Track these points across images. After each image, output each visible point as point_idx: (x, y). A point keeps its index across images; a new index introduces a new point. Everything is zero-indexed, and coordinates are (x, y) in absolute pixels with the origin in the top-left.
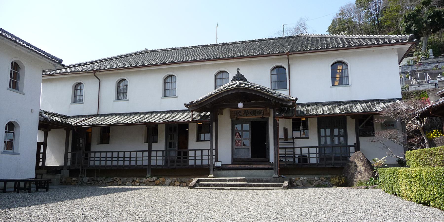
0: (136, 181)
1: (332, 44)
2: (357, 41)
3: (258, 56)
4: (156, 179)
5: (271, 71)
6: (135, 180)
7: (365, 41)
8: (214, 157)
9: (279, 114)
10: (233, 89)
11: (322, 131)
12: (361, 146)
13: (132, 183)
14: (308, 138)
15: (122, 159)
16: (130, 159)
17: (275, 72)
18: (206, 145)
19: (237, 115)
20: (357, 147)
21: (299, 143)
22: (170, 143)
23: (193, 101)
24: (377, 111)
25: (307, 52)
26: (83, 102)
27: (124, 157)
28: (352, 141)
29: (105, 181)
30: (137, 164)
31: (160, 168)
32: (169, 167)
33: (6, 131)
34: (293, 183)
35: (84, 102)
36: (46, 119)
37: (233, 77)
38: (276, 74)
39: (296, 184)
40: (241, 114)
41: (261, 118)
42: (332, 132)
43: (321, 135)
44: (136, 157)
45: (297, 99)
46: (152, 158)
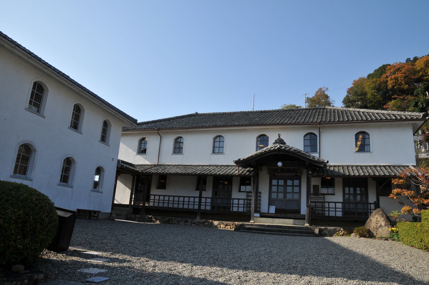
0: (189, 221)
1: (356, 117)
2: (377, 116)
4: (205, 221)
5: (304, 137)
6: (188, 220)
7: (384, 116)
9: (312, 173)
11: (347, 189)
12: (381, 205)
14: (334, 194)
15: (172, 202)
16: (169, 202)
17: (308, 137)
20: (377, 205)
21: (328, 198)
23: (240, 159)
24: (395, 175)
25: (336, 123)
27: (179, 201)
28: (372, 199)
31: (209, 212)
33: (62, 174)
34: (322, 232)
35: (184, 154)
36: (122, 166)
37: (275, 141)
38: (309, 140)
39: (324, 233)
40: (278, 171)
41: (295, 175)
42: (355, 191)
43: (346, 193)
44: (179, 201)
45: (328, 162)
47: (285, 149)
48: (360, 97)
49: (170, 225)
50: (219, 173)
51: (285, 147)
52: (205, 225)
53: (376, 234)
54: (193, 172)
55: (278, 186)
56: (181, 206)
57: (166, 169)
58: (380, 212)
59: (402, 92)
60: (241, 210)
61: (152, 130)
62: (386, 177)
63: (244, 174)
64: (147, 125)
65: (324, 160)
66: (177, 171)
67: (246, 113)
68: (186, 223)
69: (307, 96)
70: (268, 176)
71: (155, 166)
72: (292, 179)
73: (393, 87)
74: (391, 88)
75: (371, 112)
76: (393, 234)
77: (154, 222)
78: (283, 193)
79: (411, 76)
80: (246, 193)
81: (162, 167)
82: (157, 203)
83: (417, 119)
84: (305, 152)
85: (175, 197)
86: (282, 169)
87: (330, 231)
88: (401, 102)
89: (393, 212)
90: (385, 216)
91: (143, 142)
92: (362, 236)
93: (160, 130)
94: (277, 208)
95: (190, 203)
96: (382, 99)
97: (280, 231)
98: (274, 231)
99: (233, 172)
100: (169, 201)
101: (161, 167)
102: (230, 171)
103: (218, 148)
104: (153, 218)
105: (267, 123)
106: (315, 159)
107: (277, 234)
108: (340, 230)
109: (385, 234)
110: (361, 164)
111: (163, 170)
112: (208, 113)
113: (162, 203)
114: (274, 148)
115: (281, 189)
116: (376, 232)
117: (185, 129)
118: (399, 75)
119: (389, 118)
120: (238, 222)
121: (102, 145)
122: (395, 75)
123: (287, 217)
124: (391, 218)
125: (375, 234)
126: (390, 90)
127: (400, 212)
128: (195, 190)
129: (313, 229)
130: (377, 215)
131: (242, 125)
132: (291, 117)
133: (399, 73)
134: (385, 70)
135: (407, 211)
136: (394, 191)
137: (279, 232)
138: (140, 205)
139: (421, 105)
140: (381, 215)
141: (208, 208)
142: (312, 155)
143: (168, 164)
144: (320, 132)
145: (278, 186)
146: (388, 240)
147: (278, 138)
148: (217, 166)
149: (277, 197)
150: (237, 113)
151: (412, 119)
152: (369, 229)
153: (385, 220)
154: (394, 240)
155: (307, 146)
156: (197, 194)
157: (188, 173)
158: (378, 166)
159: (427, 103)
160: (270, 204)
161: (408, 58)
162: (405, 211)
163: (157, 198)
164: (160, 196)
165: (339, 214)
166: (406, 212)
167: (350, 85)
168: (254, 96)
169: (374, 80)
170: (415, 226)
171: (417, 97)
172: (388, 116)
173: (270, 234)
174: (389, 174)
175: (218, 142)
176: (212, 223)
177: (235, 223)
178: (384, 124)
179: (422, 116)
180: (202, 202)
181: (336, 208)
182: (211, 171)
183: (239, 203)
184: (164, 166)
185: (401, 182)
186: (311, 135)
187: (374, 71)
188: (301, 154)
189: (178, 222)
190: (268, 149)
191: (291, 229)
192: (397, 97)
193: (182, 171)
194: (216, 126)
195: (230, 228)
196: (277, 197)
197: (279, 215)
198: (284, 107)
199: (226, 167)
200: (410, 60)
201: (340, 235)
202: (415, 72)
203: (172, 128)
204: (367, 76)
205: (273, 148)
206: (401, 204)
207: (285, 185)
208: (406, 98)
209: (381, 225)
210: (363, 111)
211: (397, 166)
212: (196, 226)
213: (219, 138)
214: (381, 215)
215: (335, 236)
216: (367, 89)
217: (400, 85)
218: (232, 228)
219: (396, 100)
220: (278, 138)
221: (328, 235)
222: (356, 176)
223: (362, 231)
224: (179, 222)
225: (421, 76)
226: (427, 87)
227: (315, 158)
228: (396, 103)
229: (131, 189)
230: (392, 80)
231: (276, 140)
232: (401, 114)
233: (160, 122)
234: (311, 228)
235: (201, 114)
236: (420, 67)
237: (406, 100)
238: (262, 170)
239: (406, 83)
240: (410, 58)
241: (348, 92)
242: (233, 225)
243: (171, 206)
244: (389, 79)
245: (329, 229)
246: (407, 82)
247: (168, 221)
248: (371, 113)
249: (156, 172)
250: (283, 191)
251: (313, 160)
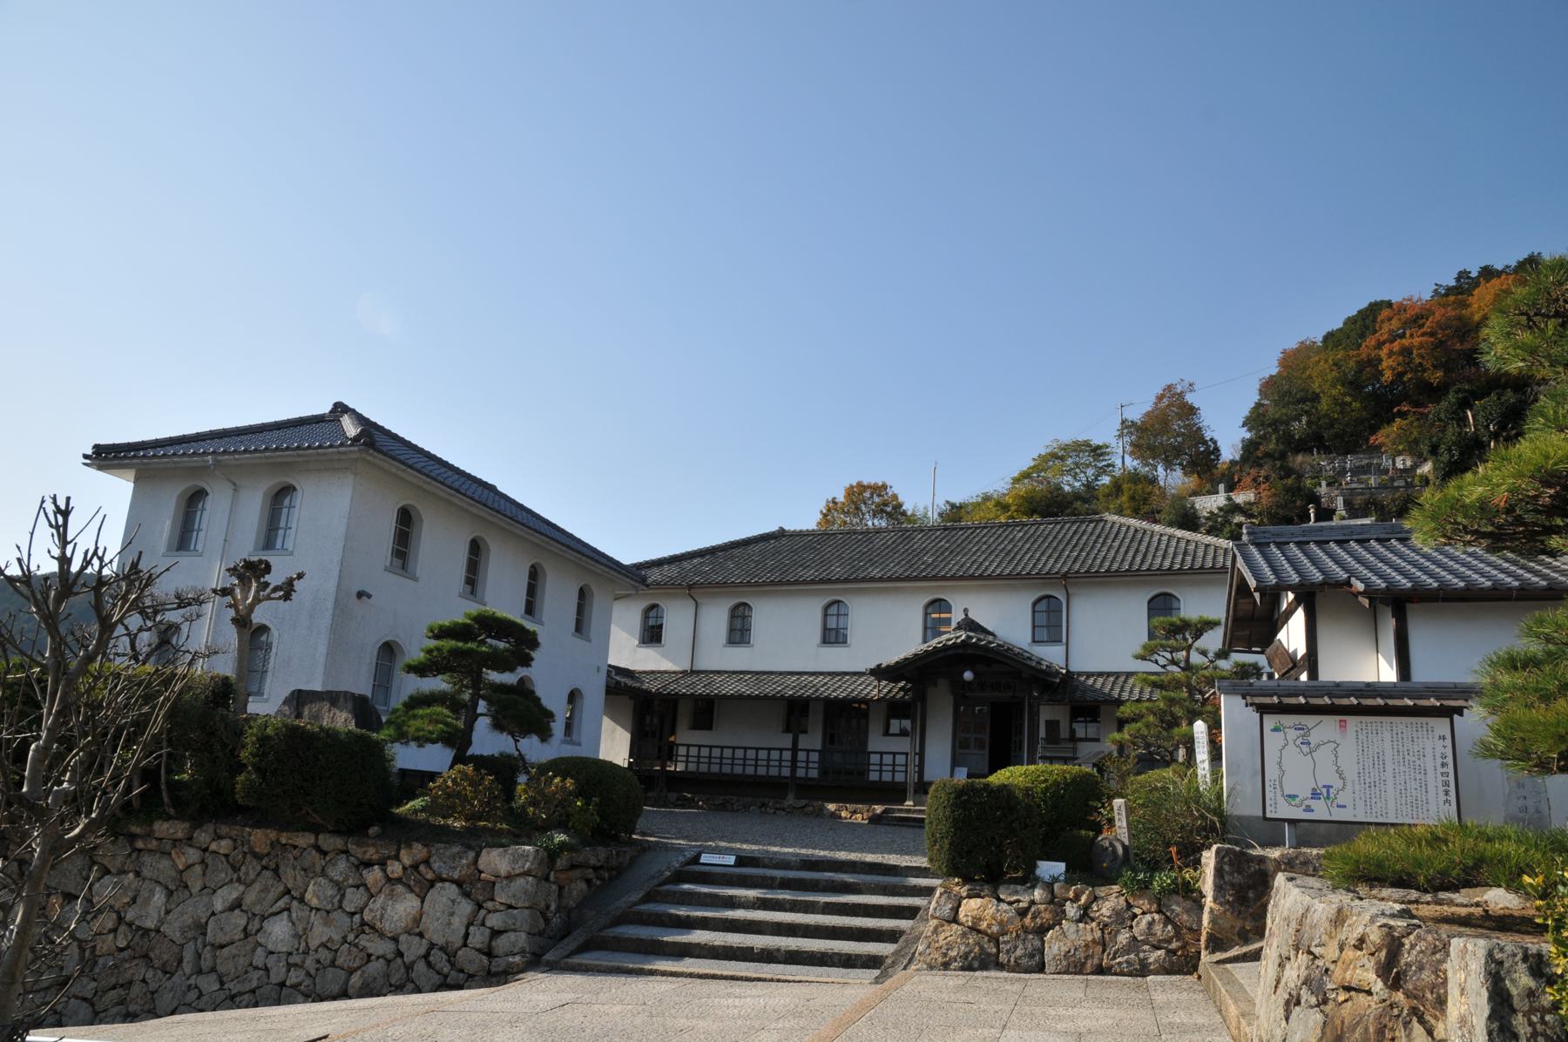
3: (1009, 577)
8: (917, 769)
17: (1042, 606)
18: (903, 745)
22: (832, 736)
27: (721, 758)
36: (618, 683)
44: (757, 760)
56: (750, 770)
68: (763, 809)
70: (951, 699)
82: (695, 765)
91: (651, 614)
118: (1417, 340)
121: (580, 642)
141: (814, 774)
156: (786, 741)
161: (1462, 269)
163: (693, 751)
164: (700, 747)
176: (822, 809)
181: (733, 759)
182: (818, 689)
187: (1345, 323)
200: (1469, 278)
213: (835, 606)
224: (746, 807)
227: (1043, 662)
229: (630, 729)
242: (868, 811)
243: (726, 769)
251: (1038, 667)
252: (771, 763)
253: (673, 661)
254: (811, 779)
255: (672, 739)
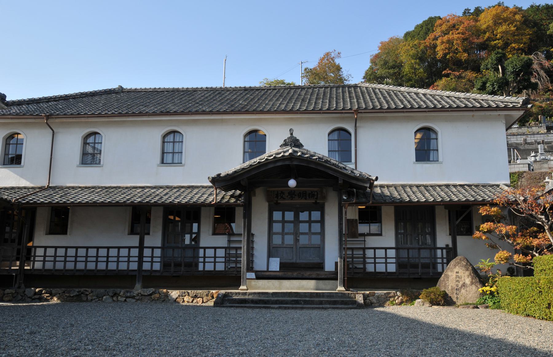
0: (120, 294)
4: (153, 292)
5: (329, 134)
6: (118, 292)
7: (461, 101)
9: (347, 198)
10: (283, 158)
13: (113, 298)
14: (380, 235)
16: (65, 259)
17: (335, 136)
19: (277, 197)
21: (372, 242)
25: (384, 111)
26: (102, 163)
29: (67, 294)
30: (206, 269)
31: (158, 274)
32: (172, 274)
37: (284, 141)
39: (369, 302)
40: (284, 195)
41: (313, 203)
46: (145, 259)
47: (303, 155)
48: (391, 71)
49: (84, 304)
50: (178, 201)
51: (303, 153)
52: (153, 300)
53: (457, 298)
54: (128, 200)
55: (283, 222)
57: (69, 196)
58: (463, 262)
59: (459, 65)
60: (220, 267)
61: (34, 118)
62: (469, 203)
63: (226, 202)
64: (18, 107)
65: (371, 176)
66: (93, 199)
67: (217, 90)
68: (115, 298)
69: (304, 66)
71: (42, 189)
72: (310, 209)
73: (445, 55)
74: (442, 57)
75: (437, 94)
76: (485, 297)
77: (47, 300)
78: (293, 235)
79: (473, 39)
80: (227, 236)
81: (59, 191)
83: (514, 108)
84: (336, 161)
85: (89, 250)
86: (292, 193)
87: (380, 298)
88: (457, 81)
89: (483, 260)
90: (470, 268)
92: (433, 303)
93: (53, 118)
94: (283, 261)
95: (154, 259)
96: (427, 75)
97: (297, 302)
98: (286, 302)
99: (205, 198)
100: (154, 258)
101: (57, 192)
102: (199, 197)
103: (171, 155)
104: (43, 292)
105: (263, 109)
106: (355, 173)
107: (293, 308)
108: (396, 294)
109: (471, 298)
110: (424, 183)
111: (62, 196)
112: (143, 87)
113: (63, 263)
114: (282, 154)
115: (290, 227)
116: (456, 296)
117: (105, 117)
118: (456, 36)
119: (470, 105)
120: (217, 290)
122: (448, 36)
123: (304, 277)
124: (479, 271)
125: (455, 300)
126: (440, 61)
127: (494, 261)
128: (128, 234)
129: (352, 295)
130: (457, 267)
131: (218, 111)
132: (303, 100)
133: (455, 32)
134: (433, 26)
135: (505, 259)
136: (483, 227)
137: (295, 304)
138: (12, 268)
139: (490, 86)
140: (465, 267)
141: (157, 266)
142: (349, 167)
143: (70, 185)
144: (356, 125)
145: (283, 222)
146: (478, 308)
147: (290, 136)
148: (171, 188)
149: (282, 243)
150: (200, 91)
151: (506, 108)
152: (445, 291)
153: (470, 274)
154: (487, 307)
155: (334, 152)
156: (134, 241)
157: (117, 202)
158: (453, 186)
159: (500, 85)
160: (270, 255)
161: (467, 8)
162: (502, 259)
164: (56, 248)
165: (392, 268)
166: (503, 261)
167: (376, 51)
168: (225, 60)
169: (416, 43)
170: (536, 283)
171: (480, 74)
172: (467, 102)
173: (280, 308)
174: (473, 199)
175: (171, 143)
176: (167, 295)
177: (211, 291)
178: (461, 115)
179: (521, 103)
180: (144, 256)
182: (162, 197)
183: (217, 256)
184: (63, 190)
185: (494, 212)
186: (340, 132)
187: (415, 28)
188: (331, 165)
189: (98, 297)
190: (272, 156)
191: (314, 297)
192: (450, 73)
193: (38, 199)
194: (168, 112)
195: (203, 302)
196: (283, 243)
197: (289, 274)
198: (265, 84)
199: (189, 190)
200: (469, 13)
201: (397, 304)
202: (479, 32)
203: (79, 114)
204: (403, 35)
205: (280, 153)
206: (492, 247)
207: (297, 221)
208: (463, 75)
209: (464, 283)
210: (423, 93)
211: (482, 186)
212: (136, 301)
213: (172, 135)
214: (465, 266)
215: (388, 305)
216: (403, 58)
217: (455, 52)
218: (207, 302)
219: (449, 77)
220: (290, 136)
221: (376, 305)
222: (422, 202)
223: (435, 296)
224: (99, 297)
225: (487, 40)
226: (501, 57)
228: (449, 83)
230: (443, 43)
231: (285, 140)
232: (486, 99)
233: (47, 102)
234: (349, 294)
235: (130, 89)
236: (486, 25)
237: (464, 78)
238: (255, 195)
239: (465, 51)
240: (469, 9)
241: (373, 61)
242: (207, 295)
243: (81, 266)
244: (438, 42)
245: (377, 295)
246: (466, 48)
247: (76, 296)
248: (437, 95)
249: (50, 202)
250: (292, 231)
251: (352, 175)
252: (99, 259)
253: (31, 183)
254: (156, 271)
255: (30, 244)
